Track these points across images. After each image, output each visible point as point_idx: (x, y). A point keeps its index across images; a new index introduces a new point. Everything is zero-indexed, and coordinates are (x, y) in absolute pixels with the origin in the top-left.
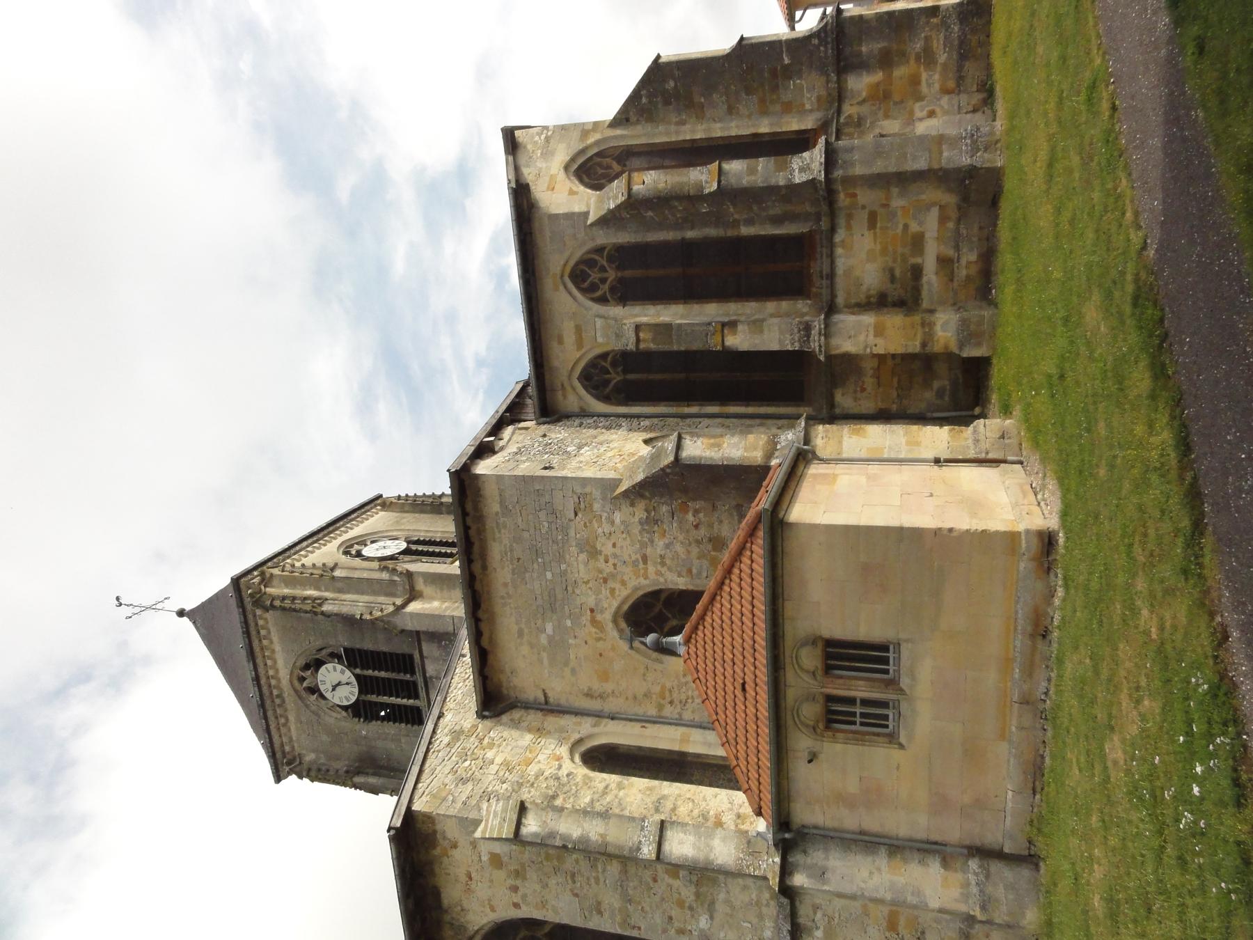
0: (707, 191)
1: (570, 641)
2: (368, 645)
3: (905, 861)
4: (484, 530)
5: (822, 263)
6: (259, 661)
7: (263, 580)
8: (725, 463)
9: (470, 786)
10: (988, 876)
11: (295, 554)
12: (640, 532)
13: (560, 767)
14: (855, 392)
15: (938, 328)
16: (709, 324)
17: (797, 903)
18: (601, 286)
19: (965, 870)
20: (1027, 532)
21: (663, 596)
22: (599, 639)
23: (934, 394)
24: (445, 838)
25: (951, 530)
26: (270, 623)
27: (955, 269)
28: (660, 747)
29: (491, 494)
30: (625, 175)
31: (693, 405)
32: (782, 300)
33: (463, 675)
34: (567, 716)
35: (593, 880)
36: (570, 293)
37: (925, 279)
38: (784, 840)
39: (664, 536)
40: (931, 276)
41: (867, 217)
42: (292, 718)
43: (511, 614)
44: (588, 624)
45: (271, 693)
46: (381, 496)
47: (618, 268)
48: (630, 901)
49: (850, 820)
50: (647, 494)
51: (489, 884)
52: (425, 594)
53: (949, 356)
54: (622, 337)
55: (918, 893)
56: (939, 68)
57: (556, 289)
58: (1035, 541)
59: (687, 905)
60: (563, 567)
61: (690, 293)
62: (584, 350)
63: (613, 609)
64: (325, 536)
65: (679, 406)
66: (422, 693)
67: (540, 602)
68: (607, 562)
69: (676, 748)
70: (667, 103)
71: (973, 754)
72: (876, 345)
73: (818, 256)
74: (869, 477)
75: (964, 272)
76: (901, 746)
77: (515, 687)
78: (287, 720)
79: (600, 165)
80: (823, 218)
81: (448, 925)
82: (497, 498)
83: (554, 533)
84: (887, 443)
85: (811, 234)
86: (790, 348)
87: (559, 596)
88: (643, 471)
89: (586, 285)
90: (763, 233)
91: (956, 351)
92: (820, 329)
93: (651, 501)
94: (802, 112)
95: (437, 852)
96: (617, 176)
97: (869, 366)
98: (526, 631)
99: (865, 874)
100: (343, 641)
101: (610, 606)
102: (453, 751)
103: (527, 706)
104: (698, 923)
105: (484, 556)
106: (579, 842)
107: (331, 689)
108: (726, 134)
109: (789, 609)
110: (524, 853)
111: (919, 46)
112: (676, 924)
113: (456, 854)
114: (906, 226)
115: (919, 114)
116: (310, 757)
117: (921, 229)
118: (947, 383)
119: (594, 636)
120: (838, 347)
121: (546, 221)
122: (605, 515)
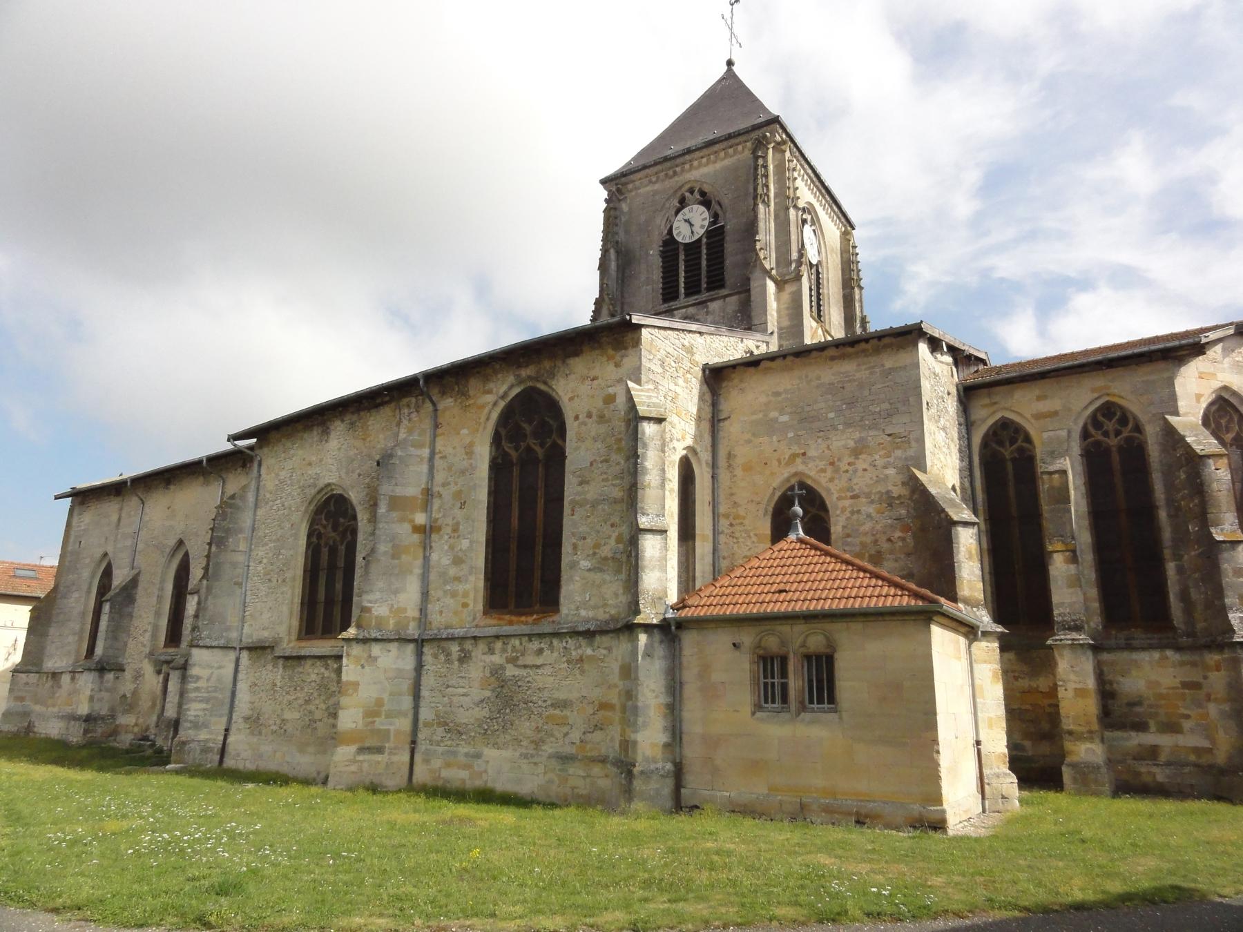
0: (1213, 530)
3: (665, 716)
4: (866, 356)
6: (705, 152)
7: (778, 144)
9: (660, 370)
10: (662, 776)
11: (801, 165)
13: (678, 440)
14: (1013, 671)
15: (1088, 745)
16: (1073, 538)
17: (611, 635)
19: (665, 760)
20: (944, 812)
21: (822, 514)
22: (779, 461)
23: (1019, 742)
24: (623, 356)
25: (938, 752)
26: (743, 153)
27: (1146, 762)
28: (697, 519)
29: (902, 358)
30: (1223, 451)
31: (986, 524)
32: (1100, 603)
33: (729, 344)
34: (710, 439)
35: (605, 476)
36: (1091, 403)
37: (1133, 734)
39: (878, 513)
40: (1136, 740)
41: (1195, 680)
42: (657, 187)
44: (791, 452)
45: (677, 166)
46: (854, 229)
47: (1120, 449)
49: (690, 675)
50: (916, 497)
52: (781, 293)
53: (1062, 755)
54: (1052, 457)
55: (645, 725)
57: (1093, 390)
58: (937, 817)
59: (597, 551)
60: (841, 427)
61: (1099, 515)
64: (817, 187)
65: (984, 512)
66: (692, 300)
68: (849, 464)
69: (698, 532)
71: (755, 767)
72: (1066, 690)
73: (1149, 636)
75: (1143, 770)
76: (753, 714)
78: (655, 183)
79: (1231, 419)
80: (1190, 639)
81: (553, 365)
82: (897, 365)
83: (871, 417)
85: (1173, 628)
86: (1056, 612)
89: (1101, 418)
91: (1068, 760)
92: (1078, 640)
93: (909, 499)
95: (611, 352)
96: (1222, 442)
97: (1042, 683)
98: (780, 399)
99: (653, 686)
100: (731, 224)
101: (810, 469)
102: (680, 350)
103: (714, 405)
105: (843, 357)
107: (686, 218)
109: (856, 626)
112: (580, 543)
113: (611, 367)
114: (1187, 717)
116: (625, 207)
117: (1185, 730)
118: (1030, 754)
120: (1062, 655)
121: (1166, 375)
122: (891, 460)
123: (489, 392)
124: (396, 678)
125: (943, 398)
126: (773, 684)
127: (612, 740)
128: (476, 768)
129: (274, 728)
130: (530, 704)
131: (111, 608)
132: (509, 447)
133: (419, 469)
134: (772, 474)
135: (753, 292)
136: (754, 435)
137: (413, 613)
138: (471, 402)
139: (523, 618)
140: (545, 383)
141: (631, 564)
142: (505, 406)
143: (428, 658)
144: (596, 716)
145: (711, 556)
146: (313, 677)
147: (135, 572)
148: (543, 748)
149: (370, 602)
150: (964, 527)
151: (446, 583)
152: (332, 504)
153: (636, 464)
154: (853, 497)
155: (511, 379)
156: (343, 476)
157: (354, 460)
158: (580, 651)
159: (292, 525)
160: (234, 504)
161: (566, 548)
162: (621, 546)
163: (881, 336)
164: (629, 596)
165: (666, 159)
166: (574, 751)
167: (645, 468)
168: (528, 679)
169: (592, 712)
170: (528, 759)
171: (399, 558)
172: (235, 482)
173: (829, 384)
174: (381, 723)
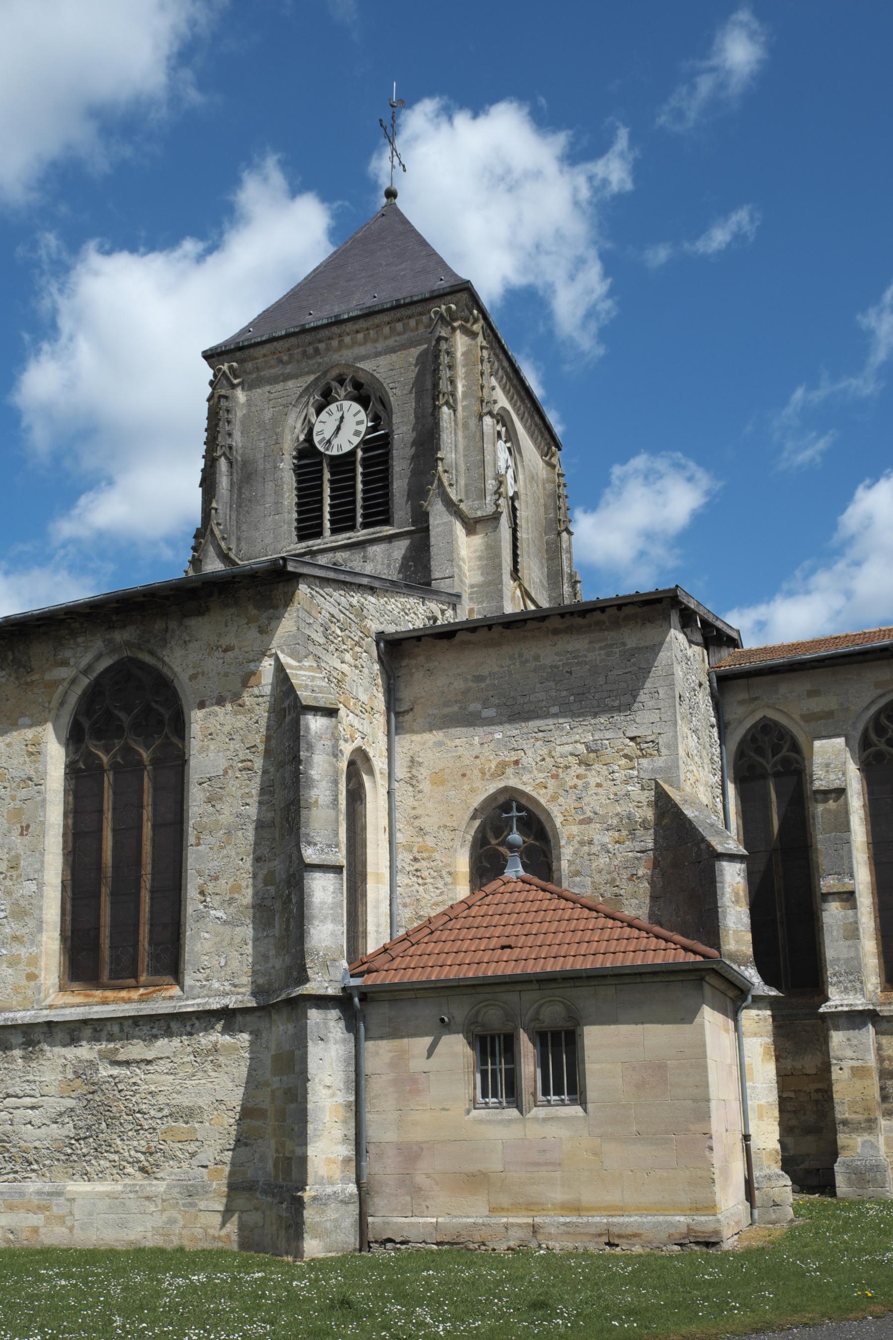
1: (476, 738)
6: (362, 324)
8: (720, 910)
9: (322, 640)
10: (344, 1202)
12: (618, 814)
13: (346, 741)
18: (883, 740)
24: (270, 619)
34: (385, 739)
36: (873, 702)
38: (350, 998)
43: (502, 667)
45: (320, 341)
48: (229, 833)
51: (223, 673)
57: (878, 685)
58: (710, 1227)
59: (236, 896)
63: (521, 787)
66: (342, 538)
67: (521, 700)
68: (578, 777)
69: (370, 869)
74: (730, 1066)
77: (412, 675)
82: (643, 644)
84: (759, 1085)
88: (696, 816)
89: (884, 721)
95: (253, 611)
98: (483, 685)
102: (347, 613)
105: (570, 630)
106: (307, 778)
113: (253, 633)
123: (65, 663)
127: (263, 1159)
130: (139, 1115)
134: (472, 790)
135: (433, 532)
138: (35, 677)
139: (124, 994)
140: (152, 653)
141: (291, 912)
142: (90, 684)
150: (730, 861)
153: (297, 774)
155: (98, 645)
161: (192, 892)
162: (272, 889)
163: (599, 608)
165: (304, 331)
167: (309, 778)
168: (133, 1080)
173: (551, 667)
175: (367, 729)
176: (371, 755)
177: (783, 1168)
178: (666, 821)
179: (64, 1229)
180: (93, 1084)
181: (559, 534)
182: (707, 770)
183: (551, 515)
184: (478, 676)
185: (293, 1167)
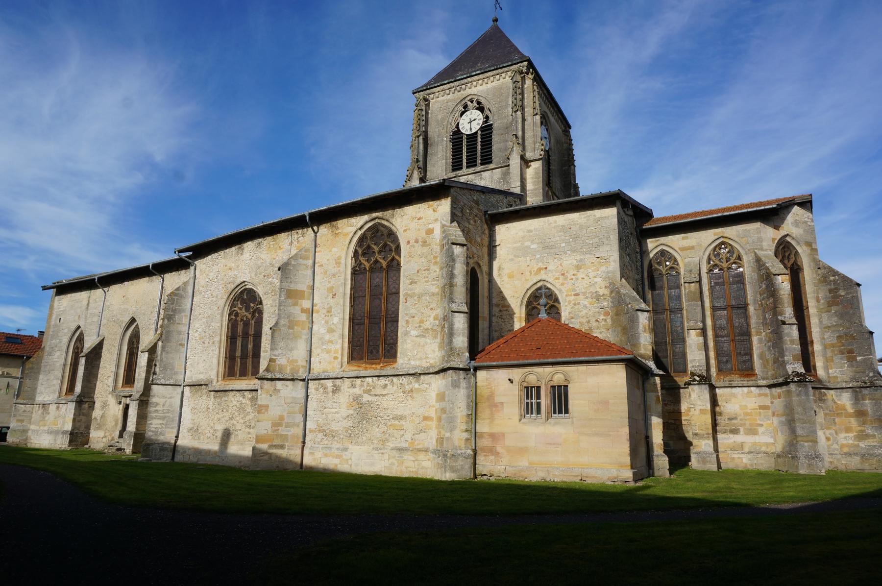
1: (528, 257)
2: (495, 138)
5: (738, 381)
12: (591, 292)
21: (556, 304)
22: (530, 272)
35: (427, 279)
37: (731, 436)
45: (463, 84)
56: (856, 443)
59: (422, 325)
62: (679, 251)
66: (471, 170)
70: (830, 291)
72: (695, 410)
73: (742, 379)
76: (520, 420)
83: (587, 247)
85: (754, 375)
87: (552, 251)
88: (627, 293)
90: (754, 348)
94: (826, 368)
96: (786, 267)
98: (531, 234)
104: (413, 330)
108: (812, 326)
110: (435, 245)
111: (870, 431)
114: (762, 425)
115: (828, 432)
117: (760, 433)
118: (672, 448)
119: (533, 270)
122: (599, 272)
124: (291, 403)
125: (628, 236)
126: (532, 403)
128: (344, 457)
129: (209, 435)
131: (86, 361)
132: (380, 258)
133: (305, 273)
136: (515, 256)
137: (302, 362)
138: (339, 231)
139: (374, 366)
143: (311, 390)
144: (421, 424)
145: (488, 330)
146: (235, 403)
147: (100, 338)
148: (387, 444)
149: (275, 355)
151: (323, 344)
152: (245, 294)
154: (575, 295)
156: (253, 275)
157: (260, 267)
158: (411, 386)
159: (218, 308)
160: (178, 294)
162: (437, 322)
164: (443, 352)
166: (407, 446)
169: (418, 422)
170: (378, 451)
171: (293, 328)
172: (174, 280)
173: (562, 226)
174: (282, 430)
175: (480, 254)
176: (481, 265)
177: (664, 452)
178: (613, 295)
179: (348, 466)
180: (361, 404)
181: (570, 166)
182: (634, 272)
183: (566, 158)
184: (530, 230)
185: (444, 442)
